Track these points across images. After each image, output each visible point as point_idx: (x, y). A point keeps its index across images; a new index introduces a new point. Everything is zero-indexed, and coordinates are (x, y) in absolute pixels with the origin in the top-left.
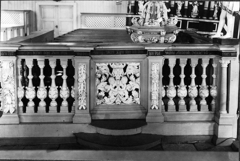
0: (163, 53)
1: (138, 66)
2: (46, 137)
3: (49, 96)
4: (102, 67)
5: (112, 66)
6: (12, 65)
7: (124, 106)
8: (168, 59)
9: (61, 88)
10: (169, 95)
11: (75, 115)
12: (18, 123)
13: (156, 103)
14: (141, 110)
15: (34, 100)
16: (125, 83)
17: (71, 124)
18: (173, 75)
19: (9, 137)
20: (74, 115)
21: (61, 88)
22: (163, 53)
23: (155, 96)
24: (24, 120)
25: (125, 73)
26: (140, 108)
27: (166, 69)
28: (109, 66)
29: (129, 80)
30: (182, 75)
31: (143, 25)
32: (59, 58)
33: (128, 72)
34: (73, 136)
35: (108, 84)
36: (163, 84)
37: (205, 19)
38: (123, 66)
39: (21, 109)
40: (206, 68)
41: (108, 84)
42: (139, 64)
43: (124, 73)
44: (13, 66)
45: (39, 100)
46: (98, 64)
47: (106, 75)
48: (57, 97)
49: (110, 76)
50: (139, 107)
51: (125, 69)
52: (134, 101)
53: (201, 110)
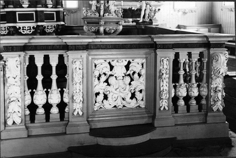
0: (24, 48)
1: (142, 64)
2: (59, 153)
3: (64, 100)
4: (102, 64)
5: (113, 64)
6: (19, 63)
7: (127, 110)
8: (34, 55)
9: (35, 92)
10: (36, 102)
11: (69, 123)
12: (27, 136)
13: (164, 103)
14: (147, 114)
15: (58, 106)
16: (128, 83)
17: (64, 135)
18: (42, 76)
19: (42, 153)
20: (68, 124)
21: (35, 92)
22: (24, 48)
23: (165, 96)
24: (34, 132)
25: (128, 72)
26: (146, 112)
27: (31, 70)
28: (109, 63)
29: (132, 80)
30: (182, 71)
31: (103, 16)
32: (33, 54)
33: (132, 68)
34: (67, 150)
35: (109, 85)
36: (173, 82)
37: (59, 8)
38: (126, 63)
39: (28, 118)
40: (56, 67)
41: (109, 85)
42: (144, 61)
43: (127, 71)
44: (21, 64)
45: (36, 107)
46: (97, 61)
47: (105, 74)
48: (30, 103)
49: (111, 75)
50: (144, 110)
51: (127, 67)
52: (138, 105)
53: (36, 121)
